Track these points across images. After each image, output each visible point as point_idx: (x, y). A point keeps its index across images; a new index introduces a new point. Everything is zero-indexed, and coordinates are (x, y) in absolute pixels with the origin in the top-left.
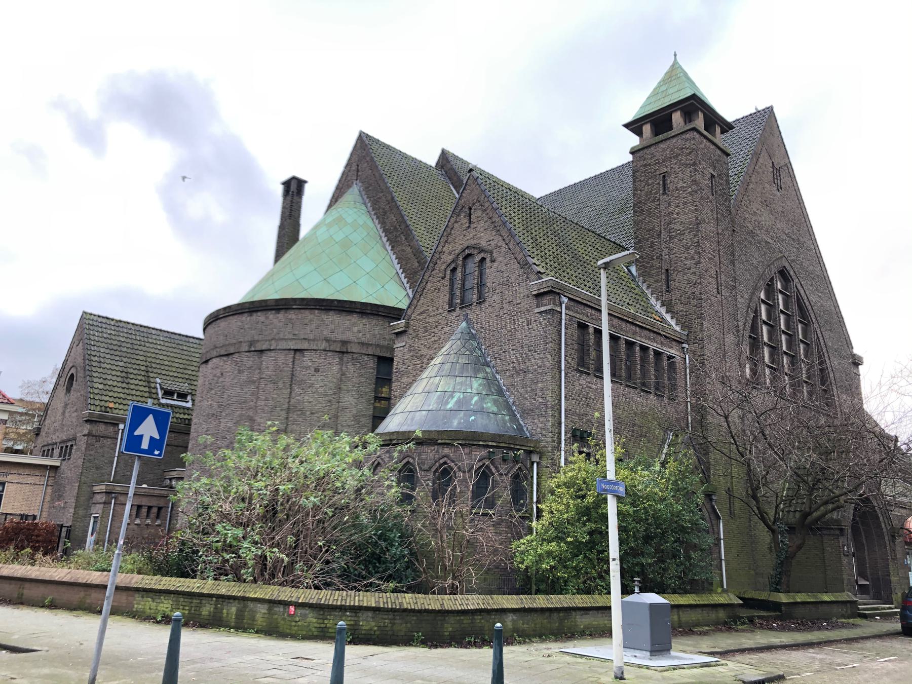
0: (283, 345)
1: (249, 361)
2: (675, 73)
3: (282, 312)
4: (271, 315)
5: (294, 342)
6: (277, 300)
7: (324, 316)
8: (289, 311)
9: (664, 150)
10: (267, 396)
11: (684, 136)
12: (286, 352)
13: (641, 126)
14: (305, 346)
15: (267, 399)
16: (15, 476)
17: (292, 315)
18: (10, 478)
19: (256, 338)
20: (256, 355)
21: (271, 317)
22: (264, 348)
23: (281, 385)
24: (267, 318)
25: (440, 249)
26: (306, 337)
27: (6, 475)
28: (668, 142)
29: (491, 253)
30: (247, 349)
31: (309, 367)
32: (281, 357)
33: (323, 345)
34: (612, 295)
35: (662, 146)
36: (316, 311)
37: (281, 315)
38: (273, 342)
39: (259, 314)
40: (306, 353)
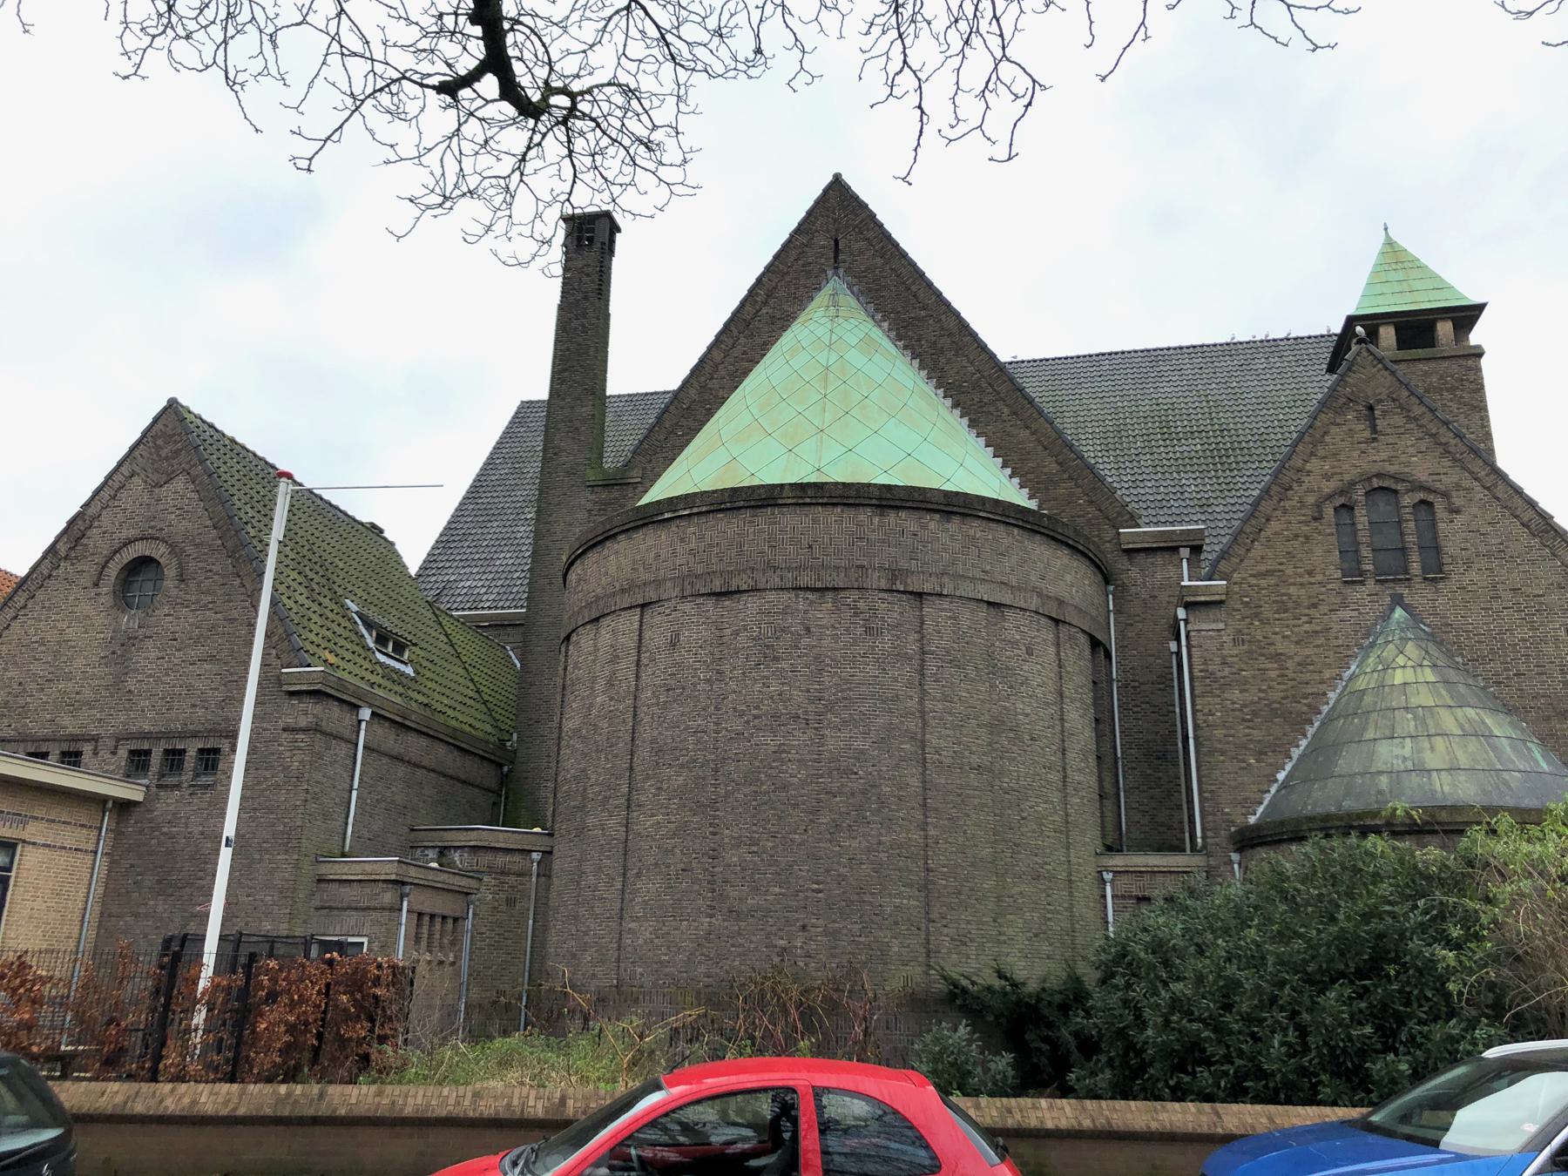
0: (966, 589)
1: (893, 611)
2: (1394, 257)
3: (956, 520)
4: (933, 523)
5: (988, 586)
6: (947, 494)
7: (1029, 545)
8: (969, 520)
9: (1426, 374)
10: (948, 691)
11: (1461, 362)
12: (973, 605)
13: (1378, 326)
14: (1006, 598)
15: (946, 699)
16: (42, 825)
17: (975, 529)
18: (32, 831)
19: (903, 564)
20: (906, 603)
21: (932, 525)
22: (927, 588)
23: (970, 670)
24: (924, 527)
25: (1297, 462)
26: (1005, 579)
27: (23, 820)
28: (1433, 364)
29: (1446, 495)
30: (883, 584)
31: (1017, 642)
32: (966, 615)
33: (1034, 602)
34: (299, 514)
35: (1420, 366)
36: (1016, 531)
37: (954, 525)
38: (946, 580)
39: (903, 514)
40: (1008, 613)
